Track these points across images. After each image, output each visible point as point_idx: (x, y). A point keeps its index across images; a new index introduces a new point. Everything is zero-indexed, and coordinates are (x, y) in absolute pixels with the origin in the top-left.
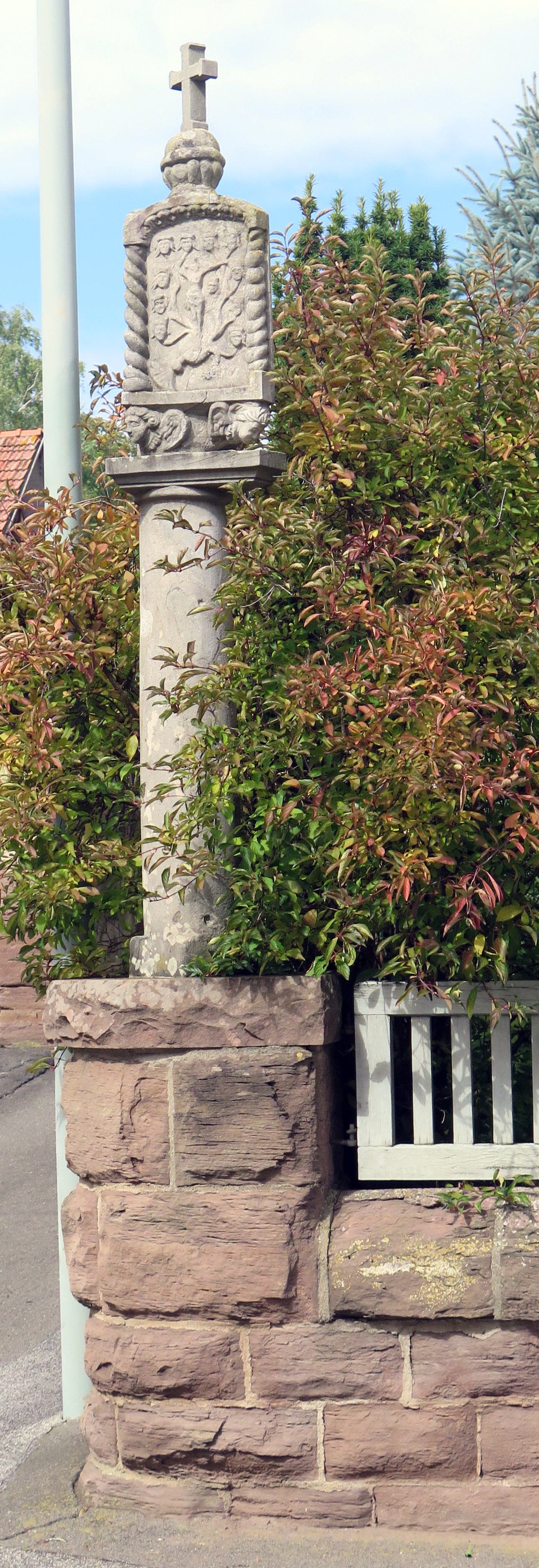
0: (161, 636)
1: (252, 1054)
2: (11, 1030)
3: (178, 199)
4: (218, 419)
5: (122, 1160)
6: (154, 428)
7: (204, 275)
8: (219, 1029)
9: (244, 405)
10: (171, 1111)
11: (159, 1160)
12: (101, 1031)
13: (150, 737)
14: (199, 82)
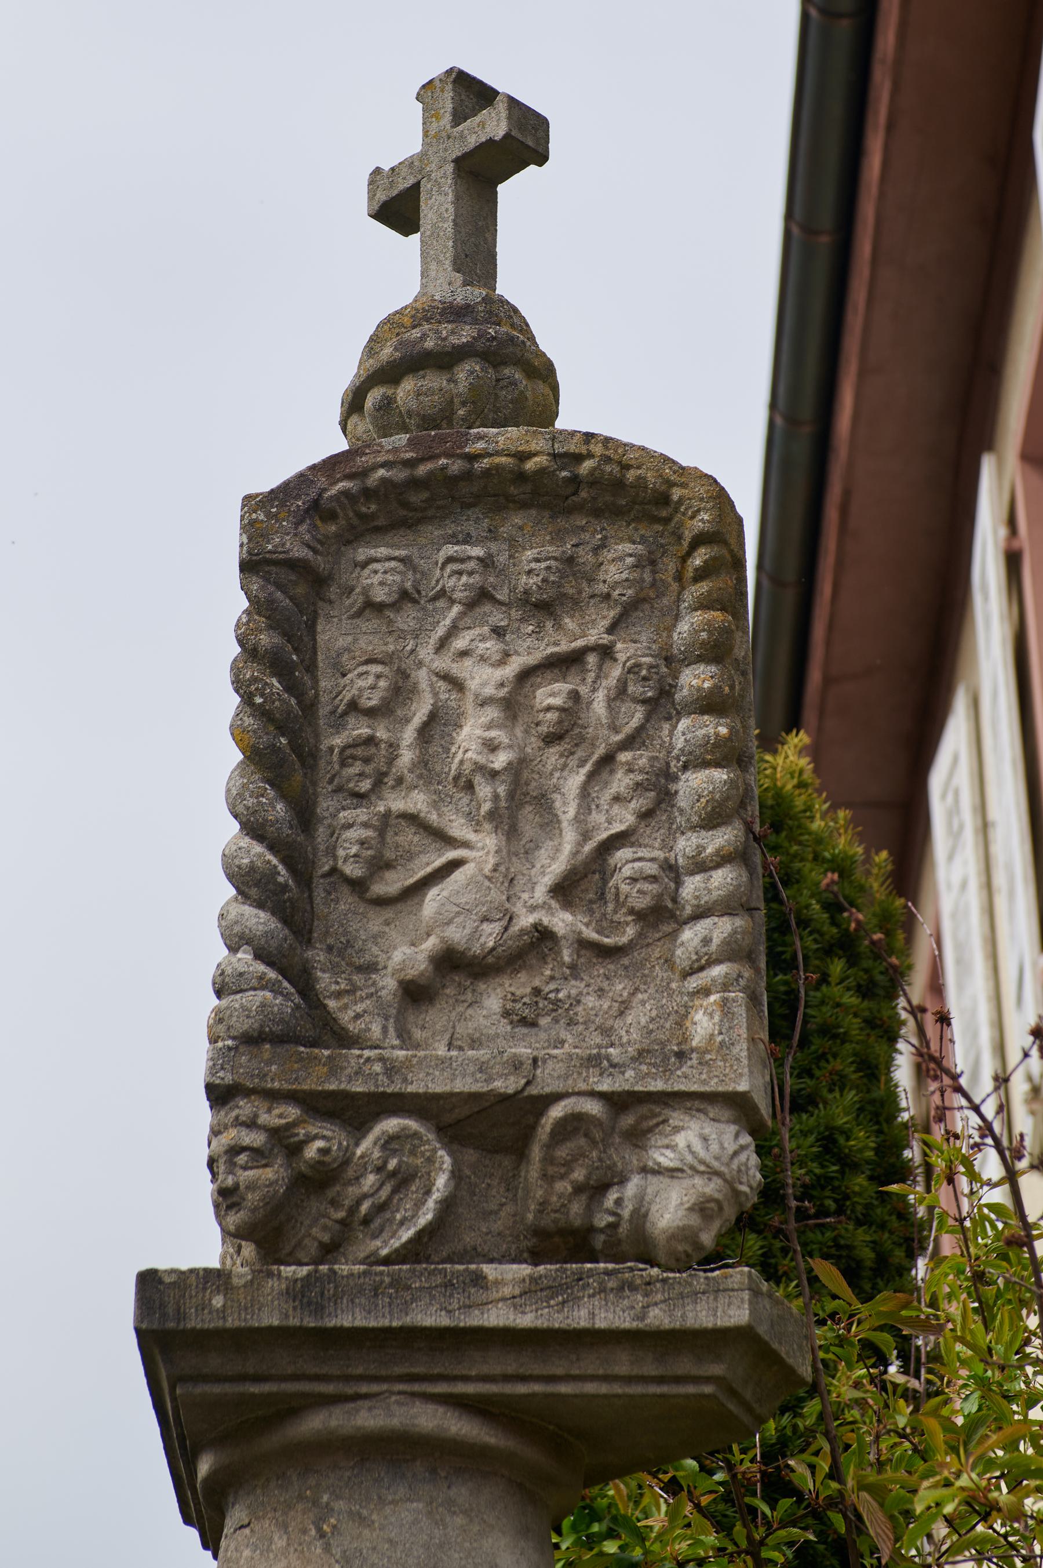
4: (568, 1165)
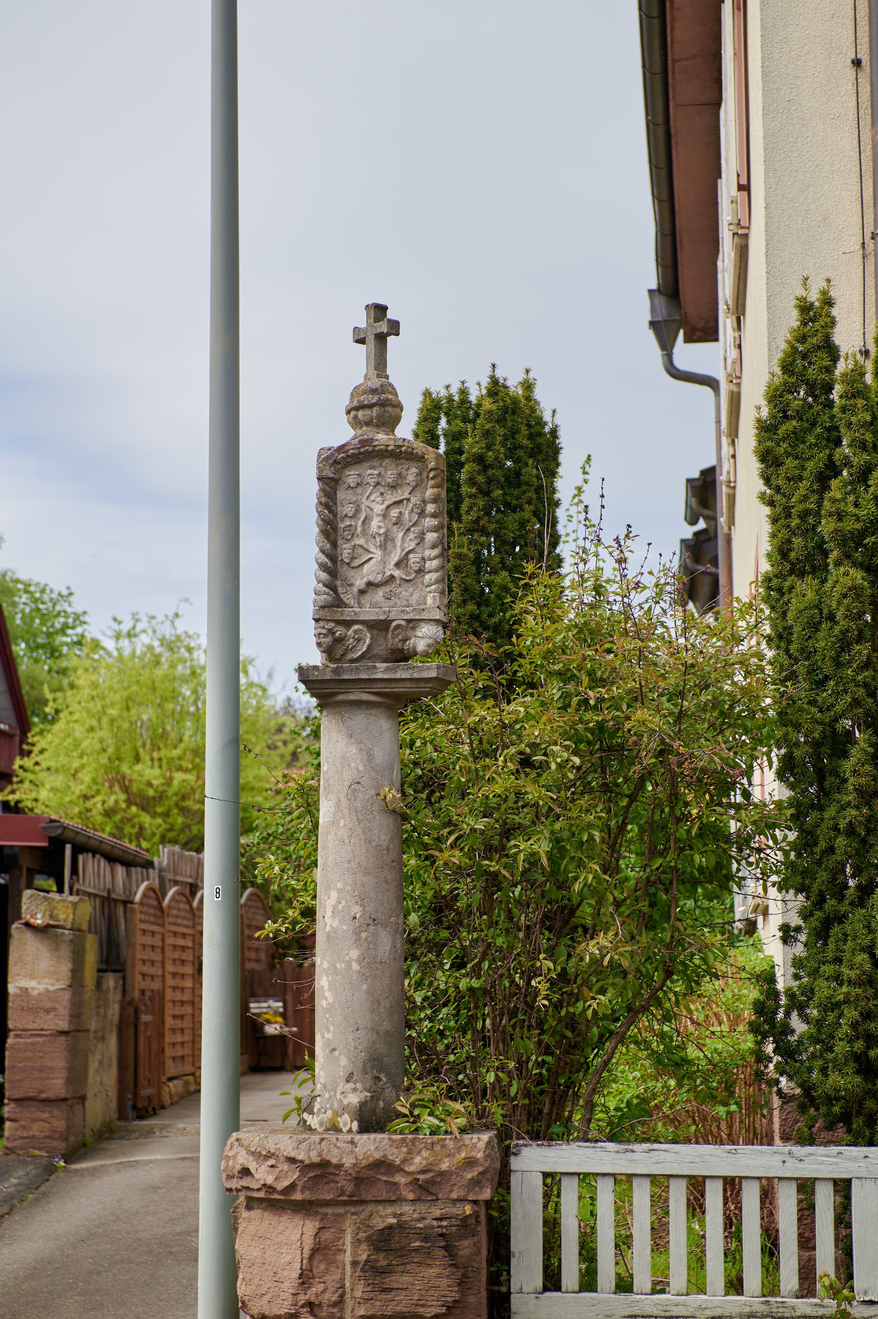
0: (342, 825)
1: (422, 1208)
2: (15, 1140)
3: (367, 440)
5: (300, 1304)
6: (341, 640)
7: (388, 507)
8: (395, 1184)
9: (422, 624)
10: (348, 1258)
11: (335, 1304)
12: (286, 1183)
13: (329, 914)
14: (381, 339)
